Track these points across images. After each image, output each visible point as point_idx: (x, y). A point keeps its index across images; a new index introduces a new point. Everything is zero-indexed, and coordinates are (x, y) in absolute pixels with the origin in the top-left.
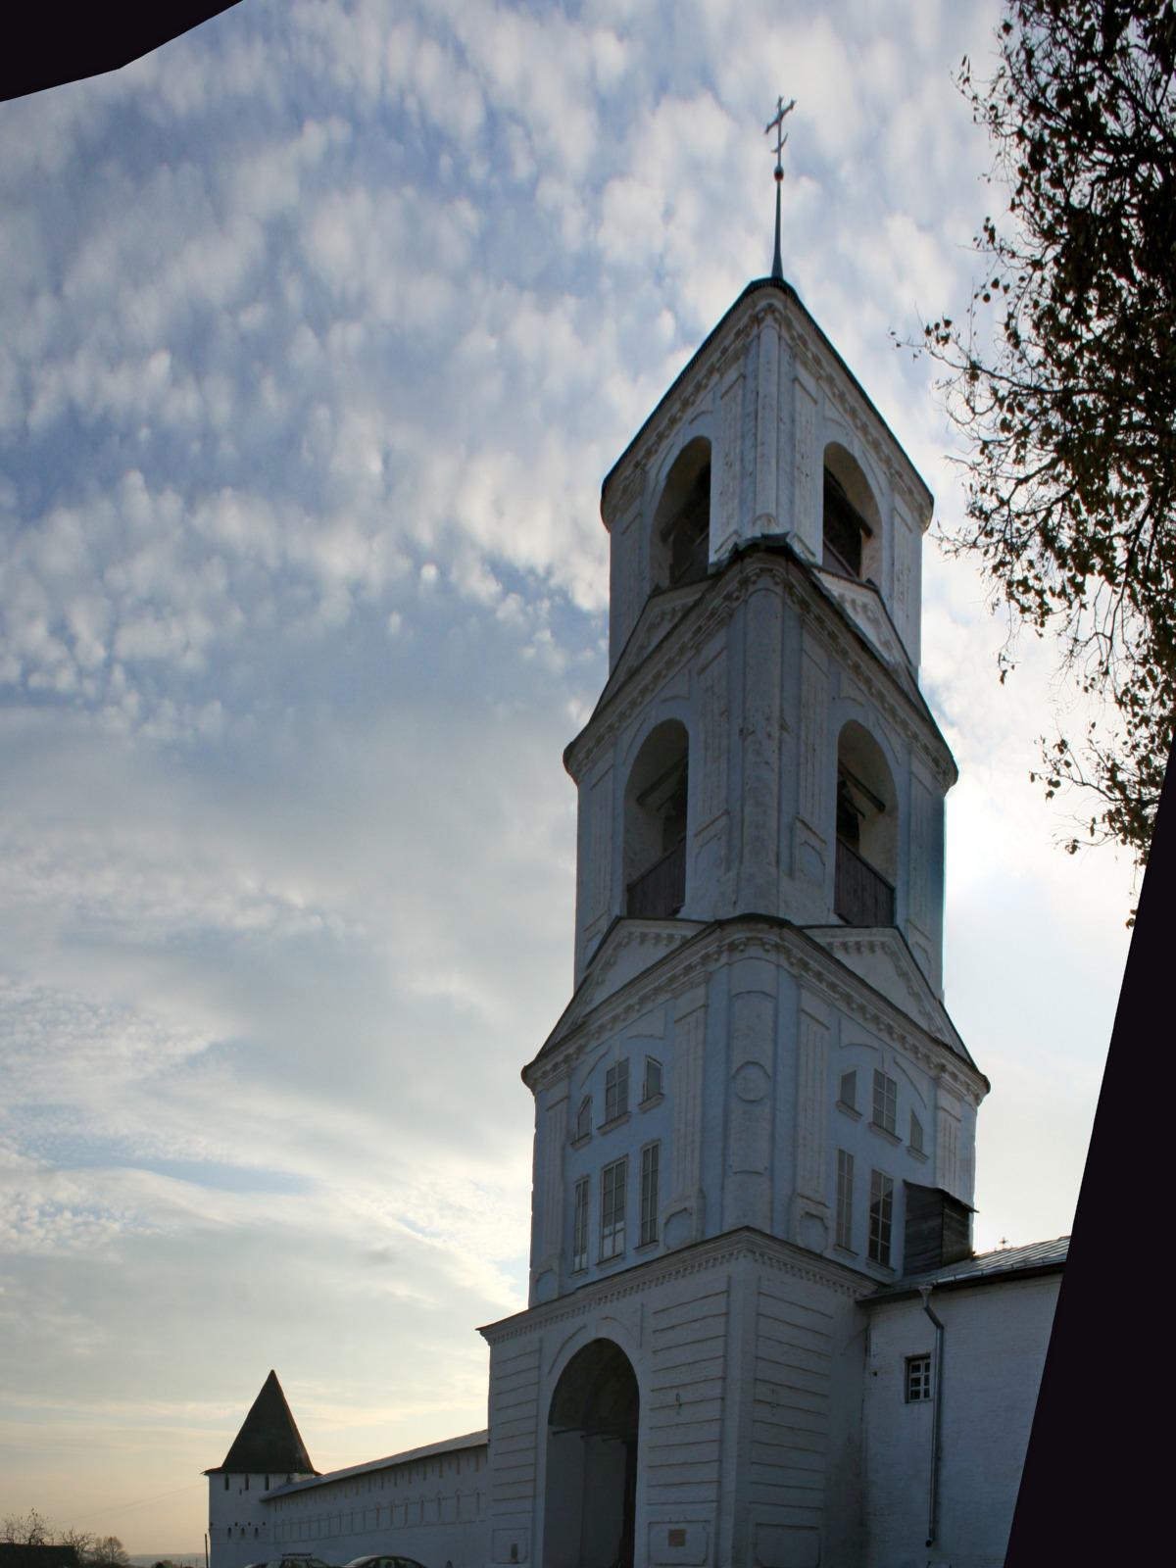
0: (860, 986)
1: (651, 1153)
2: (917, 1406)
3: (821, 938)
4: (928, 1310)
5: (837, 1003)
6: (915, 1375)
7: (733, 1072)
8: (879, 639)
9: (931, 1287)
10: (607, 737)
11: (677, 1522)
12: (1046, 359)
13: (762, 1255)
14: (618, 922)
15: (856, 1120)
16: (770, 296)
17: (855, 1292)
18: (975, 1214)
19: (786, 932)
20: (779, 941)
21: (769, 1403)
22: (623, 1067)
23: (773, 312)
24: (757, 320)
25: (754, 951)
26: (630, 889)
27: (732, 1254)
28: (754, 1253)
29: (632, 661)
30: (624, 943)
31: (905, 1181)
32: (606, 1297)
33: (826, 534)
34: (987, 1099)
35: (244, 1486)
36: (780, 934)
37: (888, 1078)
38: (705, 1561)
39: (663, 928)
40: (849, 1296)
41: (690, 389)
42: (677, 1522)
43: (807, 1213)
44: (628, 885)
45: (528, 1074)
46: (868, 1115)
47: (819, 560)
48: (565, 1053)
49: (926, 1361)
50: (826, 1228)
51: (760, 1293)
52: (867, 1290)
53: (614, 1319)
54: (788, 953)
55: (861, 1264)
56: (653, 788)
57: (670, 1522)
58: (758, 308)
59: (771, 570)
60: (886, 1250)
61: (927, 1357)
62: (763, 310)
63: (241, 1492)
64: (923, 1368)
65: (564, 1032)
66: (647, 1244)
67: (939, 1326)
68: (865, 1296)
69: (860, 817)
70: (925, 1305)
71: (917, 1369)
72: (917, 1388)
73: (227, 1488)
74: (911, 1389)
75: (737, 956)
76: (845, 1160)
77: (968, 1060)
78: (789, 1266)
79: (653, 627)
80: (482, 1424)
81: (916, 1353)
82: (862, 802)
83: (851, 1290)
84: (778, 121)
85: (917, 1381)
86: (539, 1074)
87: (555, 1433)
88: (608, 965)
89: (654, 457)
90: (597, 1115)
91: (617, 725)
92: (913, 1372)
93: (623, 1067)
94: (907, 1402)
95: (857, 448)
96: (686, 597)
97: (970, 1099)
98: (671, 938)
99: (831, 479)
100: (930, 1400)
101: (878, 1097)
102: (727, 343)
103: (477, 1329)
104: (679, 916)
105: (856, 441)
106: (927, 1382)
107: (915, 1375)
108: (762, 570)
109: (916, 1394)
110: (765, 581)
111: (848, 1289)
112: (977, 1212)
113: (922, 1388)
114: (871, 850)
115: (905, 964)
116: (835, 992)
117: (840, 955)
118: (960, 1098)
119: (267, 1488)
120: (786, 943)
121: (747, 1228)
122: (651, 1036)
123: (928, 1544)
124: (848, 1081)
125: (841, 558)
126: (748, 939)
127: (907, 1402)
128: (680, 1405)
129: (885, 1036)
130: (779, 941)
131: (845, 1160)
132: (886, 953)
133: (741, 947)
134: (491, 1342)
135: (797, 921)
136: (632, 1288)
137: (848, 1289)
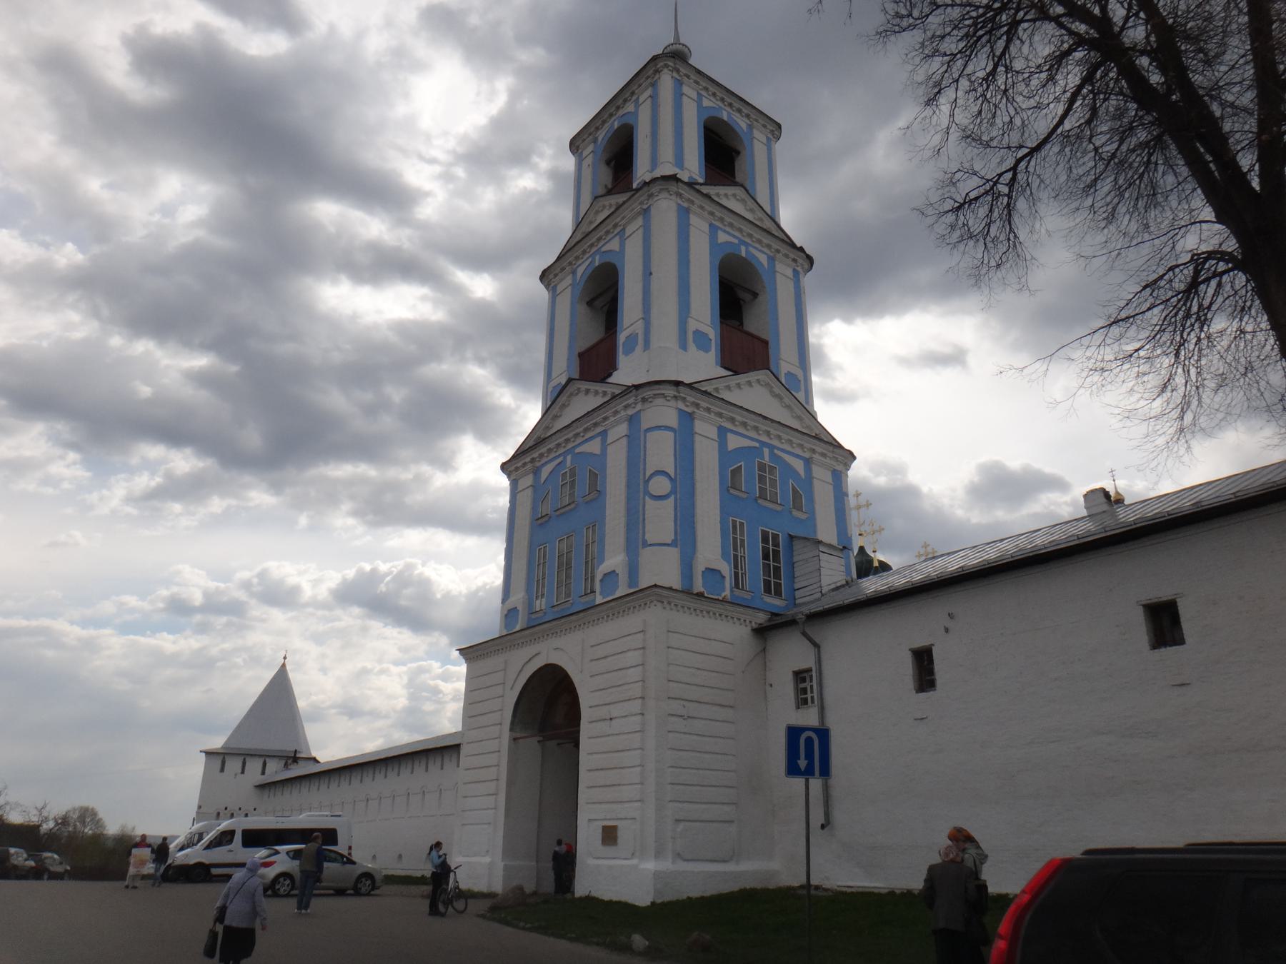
4: (804, 634)
6: (802, 685)
10: (567, 268)
11: (610, 819)
13: (669, 603)
16: (665, 60)
17: (750, 622)
19: (681, 388)
20: (676, 393)
21: (681, 716)
23: (667, 68)
25: (660, 401)
27: (646, 604)
28: (663, 602)
29: (585, 228)
30: (575, 393)
32: (557, 632)
33: (706, 161)
35: (240, 771)
40: (746, 626)
42: (610, 819)
44: (581, 355)
47: (701, 180)
48: (540, 452)
51: (669, 631)
52: (762, 618)
53: (562, 649)
56: (601, 295)
58: (658, 66)
59: (667, 189)
60: (778, 586)
61: (809, 670)
62: (662, 67)
63: (236, 775)
64: (808, 680)
65: (531, 443)
67: (816, 646)
68: (760, 624)
69: (741, 302)
71: (804, 680)
72: (805, 696)
73: (222, 770)
74: (800, 697)
75: (647, 405)
77: (834, 442)
79: (597, 212)
80: (460, 729)
83: (748, 621)
85: (804, 691)
86: (513, 468)
87: (515, 739)
88: (564, 406)
89: (600, 132)
91: (574, 262)
92: (801, 683)
96: (620, 198)
98: (605, 393)
100: (815, 706)
102: (641, 82)
103: (457, 650)
104: (610, 380)
107: (802, 685)
109: (805, 702)
110: (664, 195)
111: (745, 621)
113: (809, 696)
119: (263, 773)
120: (681, 394)
121: (655, 586)
123: (823, 827)
130: (676, 393)
132: (762, 385)
136: (575, 627)
137: (745, 621)
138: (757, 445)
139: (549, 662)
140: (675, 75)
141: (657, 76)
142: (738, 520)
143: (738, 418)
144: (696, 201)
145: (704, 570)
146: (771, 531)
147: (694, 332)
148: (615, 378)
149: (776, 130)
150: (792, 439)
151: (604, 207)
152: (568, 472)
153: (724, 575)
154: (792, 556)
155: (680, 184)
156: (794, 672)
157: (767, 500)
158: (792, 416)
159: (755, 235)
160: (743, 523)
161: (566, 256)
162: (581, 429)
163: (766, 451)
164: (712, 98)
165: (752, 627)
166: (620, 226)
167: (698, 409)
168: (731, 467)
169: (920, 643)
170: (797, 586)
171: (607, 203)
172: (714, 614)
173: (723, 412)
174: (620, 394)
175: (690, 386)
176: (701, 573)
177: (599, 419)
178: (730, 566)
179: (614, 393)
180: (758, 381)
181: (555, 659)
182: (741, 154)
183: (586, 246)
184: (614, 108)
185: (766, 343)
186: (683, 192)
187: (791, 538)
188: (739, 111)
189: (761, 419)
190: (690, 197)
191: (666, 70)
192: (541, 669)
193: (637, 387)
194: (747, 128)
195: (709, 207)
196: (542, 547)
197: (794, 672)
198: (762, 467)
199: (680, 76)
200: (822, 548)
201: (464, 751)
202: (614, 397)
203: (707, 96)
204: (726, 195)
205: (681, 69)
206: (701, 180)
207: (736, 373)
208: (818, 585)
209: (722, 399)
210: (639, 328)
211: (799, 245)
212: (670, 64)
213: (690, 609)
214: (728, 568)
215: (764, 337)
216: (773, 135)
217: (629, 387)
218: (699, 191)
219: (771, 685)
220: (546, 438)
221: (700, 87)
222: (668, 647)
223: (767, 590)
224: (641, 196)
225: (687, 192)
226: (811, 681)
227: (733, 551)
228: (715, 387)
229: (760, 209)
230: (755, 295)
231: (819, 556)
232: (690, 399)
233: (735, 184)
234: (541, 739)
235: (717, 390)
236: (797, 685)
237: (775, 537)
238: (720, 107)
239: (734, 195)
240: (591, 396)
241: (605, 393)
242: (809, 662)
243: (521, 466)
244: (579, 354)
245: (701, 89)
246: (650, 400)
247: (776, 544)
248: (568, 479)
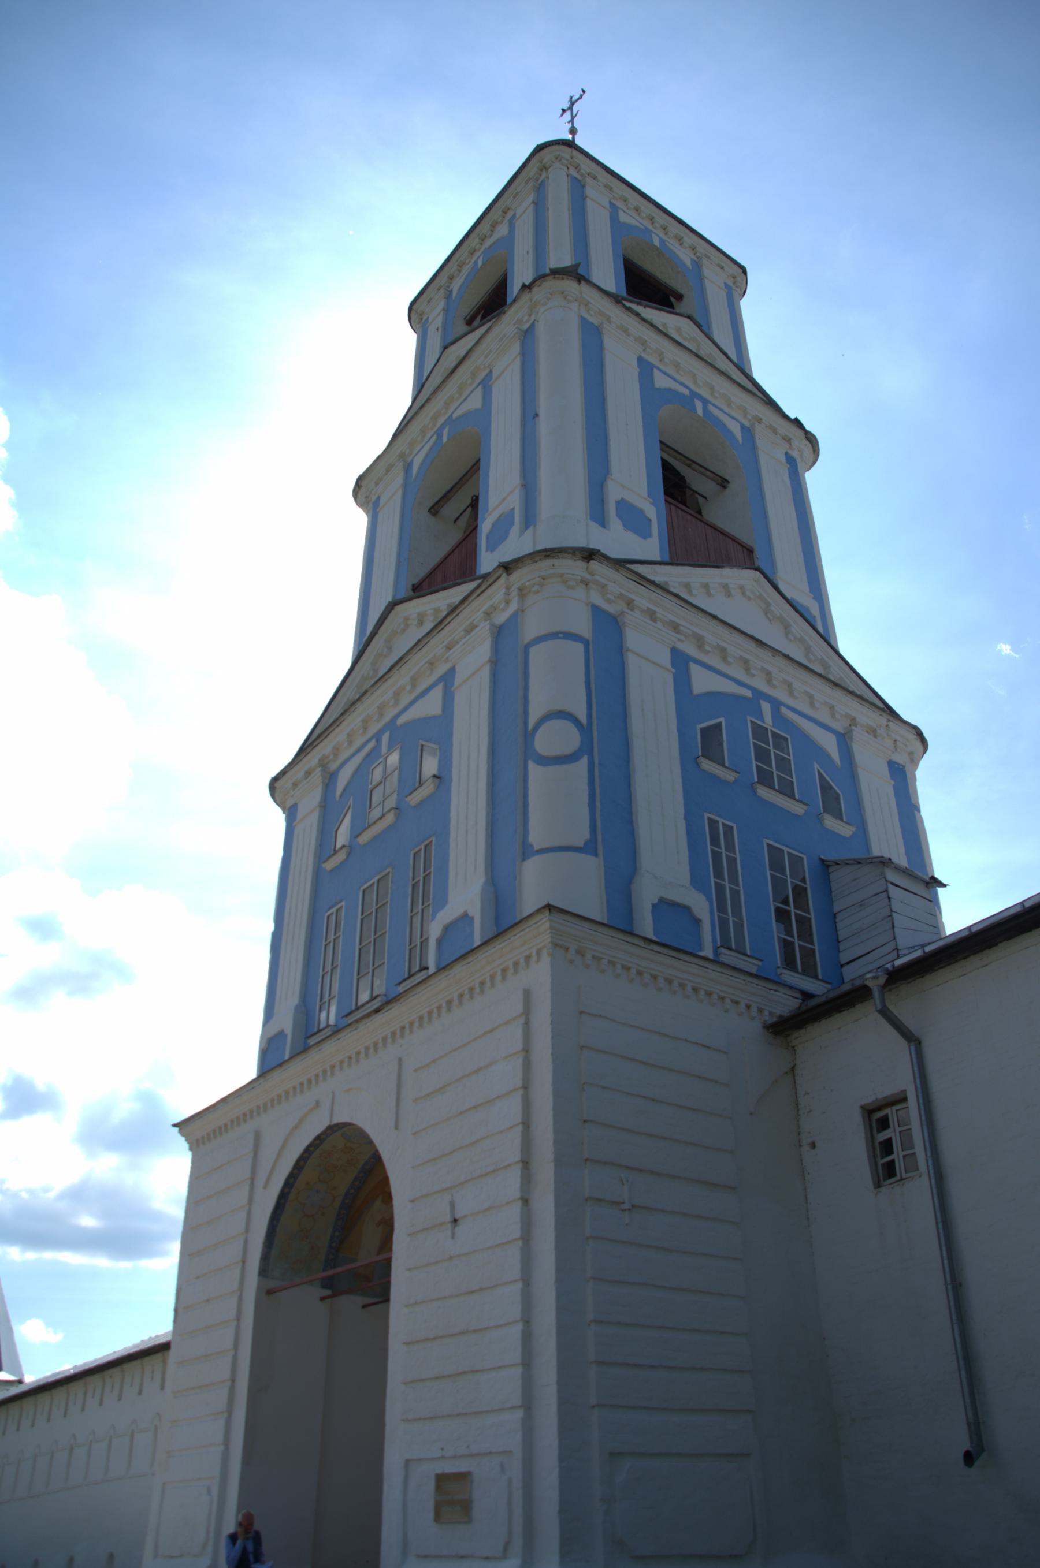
4: (885, 1013)
14: (392, 609)
17: (760, 1010)
18: (940, 890)
19: (594, 565)
20: (588, 577)
24: (544, 168)
28: (567, 949)
36: (587, 568)
38: (507, 1544)
40: (753, 1019)
45: (275, 785)
52: (785, 1004)
60: (809, 955)
61: (901, 1099)
64: (893, 1121)
67: (913, 1039)
69: (701, 500)
70: (879, 1007)
81: (880, 1096)
83: (754, 1009)
84: (571, 108)
85: (887, 1147)
87: (269, 1292)
92: (879, 1132)
94: (878, 1185)
103: (175, 1125)
111: (748, 1007)
112: (944, 886)
120: (597, 577)
123: (969, 1458)
132: (749, 599)
133: (536, 588)
134: (195, 1146)
137: (748, 1007)
138: (748, 693)
140: (573, 172)
141: (544, 175)
142: (721, 821)
145: (656, 901)
146: (786, 849)
147: (618, 503)
154: (831, 902)
156: (862, 1107)
160: (731, 828)
163: (766, 707)
168: (700, 723)
170: (844, 958)
176: (650, 907)
178: (710, 899)
184: (477, 240)
187: (826, 865)
189: (751, 646)
194: (692, 265)
196: (334, 910)
198: (760, 732)
199: (582, 175)
200: (891, 876)
203: (625, 209)
208: (891, 946)
210: (515, 501)
211: (793, 417)
214: (706, 904)
219: (813, 1145)
222: (581, 1012)
223: (789, 962)
227: (712, 844)
230: (724, 483)
231: (887, 891)
236: (872, 1137)
237: (795, 861)
238: (647, 228)
242: (904, 1080)
244: (413, 585)
246: (534, 589)
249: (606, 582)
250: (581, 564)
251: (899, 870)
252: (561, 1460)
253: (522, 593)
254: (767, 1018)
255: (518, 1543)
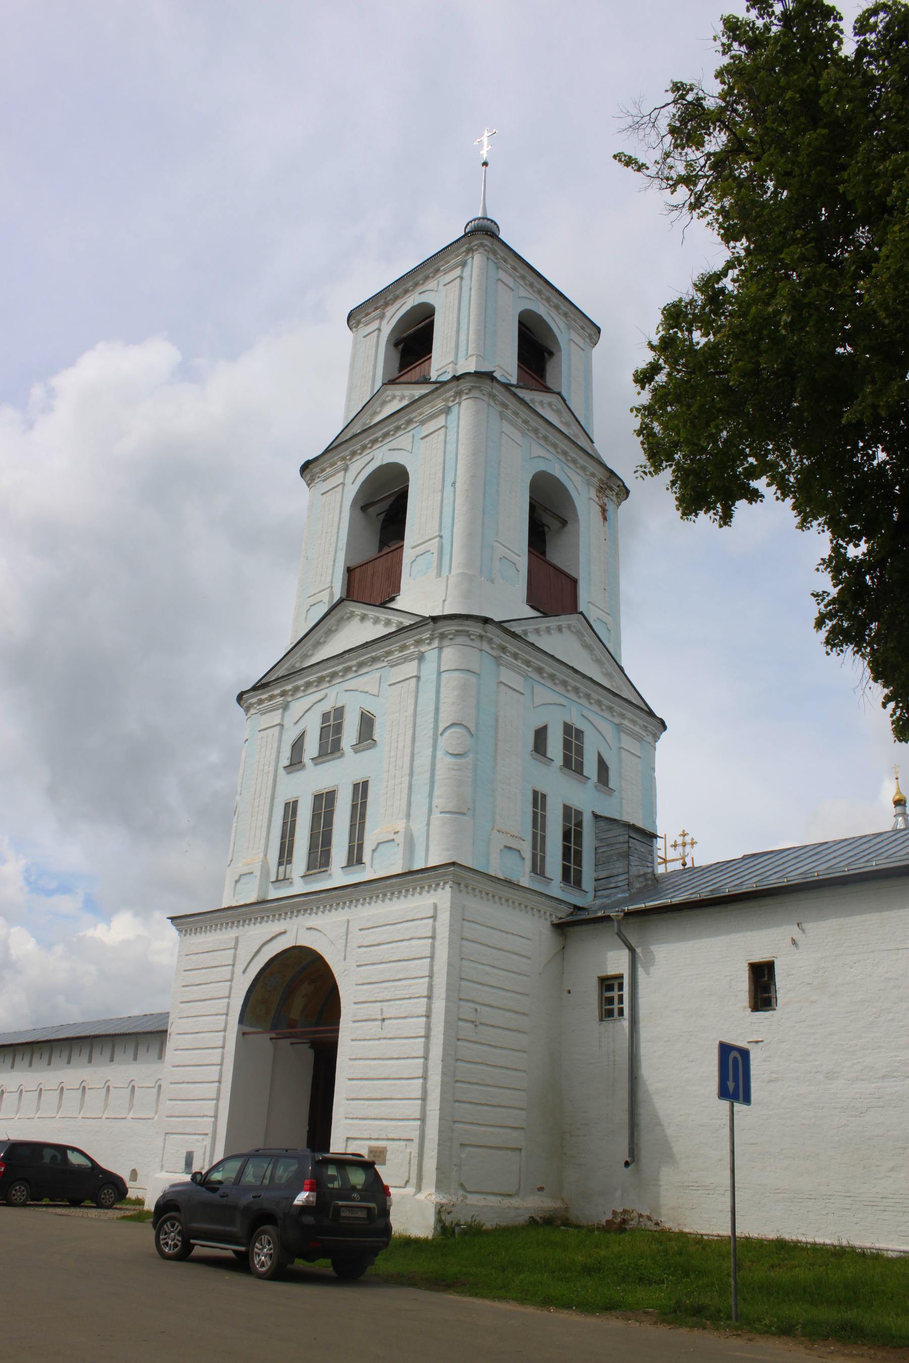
0: (550, 660)
1: (361, 790)
2: (611, 1024)
3: (516, 628)
4: (620, 934)
5: (530, 674)
6: (609, 994)
7: (440, 731)
8: (562, 422)
9: (622, 914)
10: (339, 463)
12: (686, 100)
15: (548, 765)
17: (551, 915)
19: (489, 627)
22: (339, 712)
23: (484, 247)
25: (460, 639)
26: (350, 571)
28: (459, 884)
31: (593, 813)
34: (664, 735)
37: (576, 728)
38: (407, 1182)
39: (382, 614)
40: (546, 919)
41: (421, 277)
42: (377, 1139)
43: (506, 847)
46: (559, 761)
47: (514, 381)
49: (620, 981)
50: (524, 859)
52: (563, 913)
54: (490, 641)
55: (556, 888)
57: (370, 1139)
58: (473, 244)
59: (480, 387)
60: (579, 873)
61: (621, 977)
66: (295, 764)
67: (632, 951)
68: (561, 918)
69: (546, 529)
71: (610, 988)
76: (539, 800)
78: (490, 895)
82: (547, 519)
85: (610, 1001)
87: (244, 1034)
90: (311, 748)
93: (339, 712)
94: (601, 1020)
95: (542, 309)
97: (649, 738)
99: (523, 328)
101: (567, 745)
103: (168, 918)
104: (392, 605)
105: (541, 306)
106: (621, 1000)
107: (609, 994)
108: (473, 387)
109: (610, 1013)
111: (545, 913)
113: (616, 1006)
114: (557, 556)
115: (589, 639)
116: (528, 667)
117: (531, 638)
118: (640, 739)
120: (488, 634)
122: (367, 692)
123: (627, 1164)
124: (541, 735)
125: (527, 370)
126: (457, 631)
127: (601, 1020)
128: (383, 1020)
129: (573, 696)
131: (539, 800)
132: (572, 632)
133: (451, 636)
135: (496, 619)
137: (545, 913)
139: (299, 944)
143: (548, 669)
144: (511, 406)
148: (398, 604)
149: (595, 334)
150: (601, 699)
151: (394, 397)
152: (332, 713)
153: (524, 856)
155: (495, 384)
156: (599, 977)
157: (571, 769)
158: (602, 673)
159: (571, 453)
161: (340, 449)
162: (355, 662)
164: (528, 288)
165: (552, 921)
166: (416, 422)
167: (504, 653)
169: (759, 957)
171: (398, 393)
172: (514, 903)
173: (531, 659)
174: (411, 625)
175: (499, 624)
177: (380, 652)
179: (401, 623)
180: (569, 627)
181: (306, 941)
182: (555, 357)
183: (366, 441)
185: (574, 582)
186: (497, 393)
188: (557, 308)
189: (571, 672)
190: (504, 400)
191: (481, 250)
192: (285, 951)
193: (435, 619)
195: (524, 413)
197: (599, 977)
199: (497, 259)
201: (172, 1042)
202: (402, 630)
204: (541, 403)
205: (499, 251)
206: (514, 381)
207: (546, 615)
208: (626, 876)
209: (533, 644)
212: (486, 242)
213: (487, 894)
215: (573, 574)
216: (590, 339)
217: (425, 618)
218: (515, 395)
219: (569, 992)
220: (303, 669)
221: (518, 274)
224: (446, 392)
225: (499, 392)
226: (621, 987)
228: (524, 628)
229: (577, 424)
230: (564, 523)
232: (497, 640)
233: (548, 390)
234: (274, 1035)
235: (525, 632)
236: (602, 1007)
239: (550, 404)
240: (369, 624)
241: (388, 623)
243: (266, 699)
245: (518, 277)
247: (579, 824)
248: (332, 722)
249: (493, 637)
250: (480, 625)
251: (632, 1065)
252: (439, 1145)
253: (443, 636)
254: (554, 919)
255: (413, 1181)
